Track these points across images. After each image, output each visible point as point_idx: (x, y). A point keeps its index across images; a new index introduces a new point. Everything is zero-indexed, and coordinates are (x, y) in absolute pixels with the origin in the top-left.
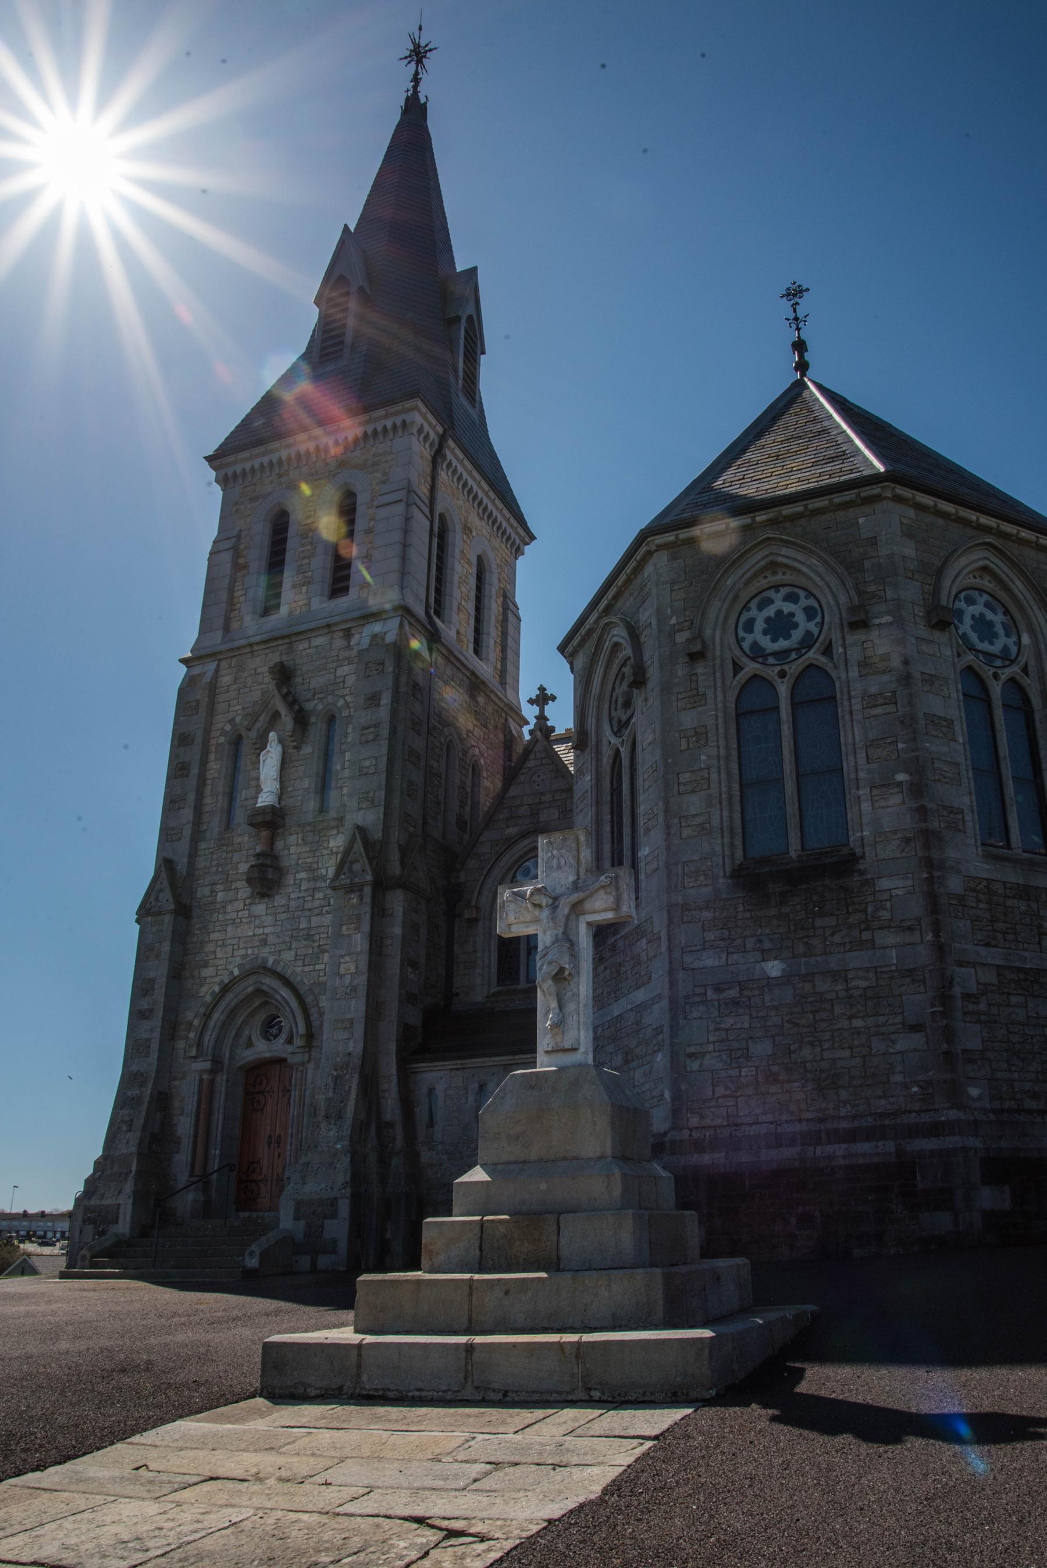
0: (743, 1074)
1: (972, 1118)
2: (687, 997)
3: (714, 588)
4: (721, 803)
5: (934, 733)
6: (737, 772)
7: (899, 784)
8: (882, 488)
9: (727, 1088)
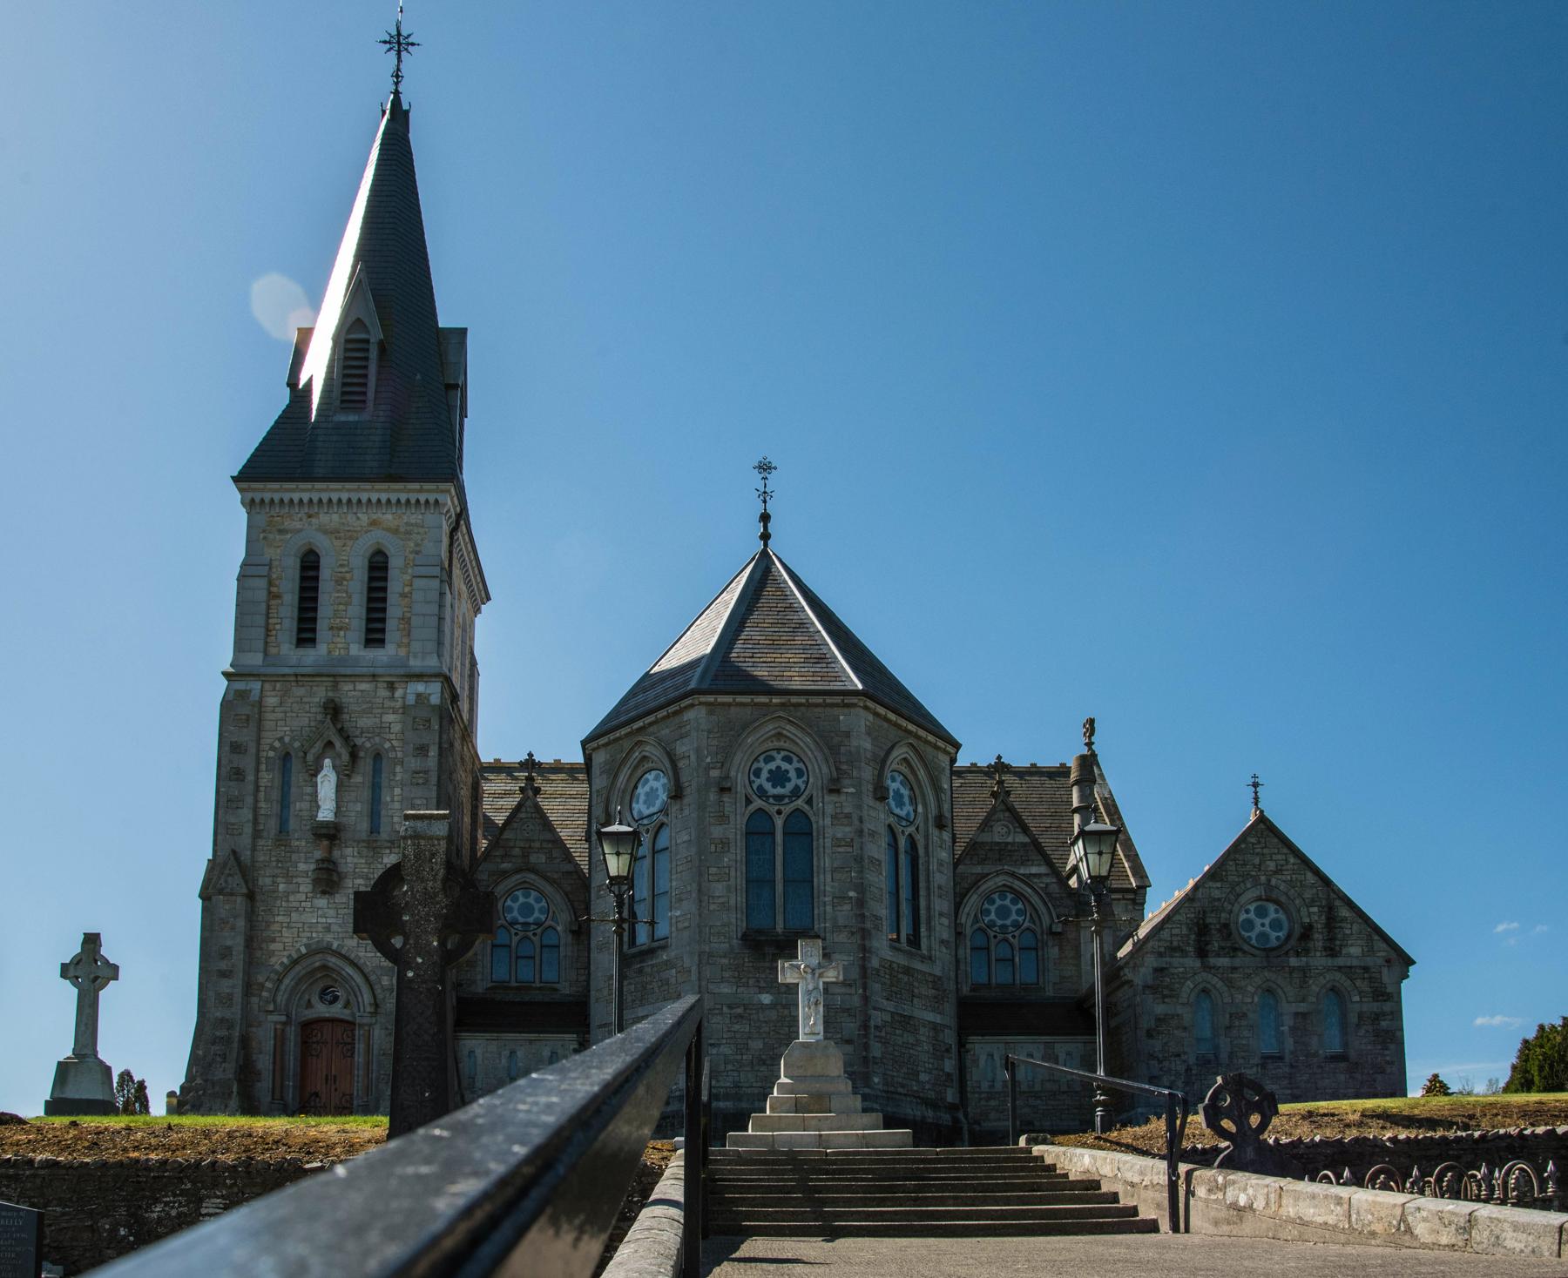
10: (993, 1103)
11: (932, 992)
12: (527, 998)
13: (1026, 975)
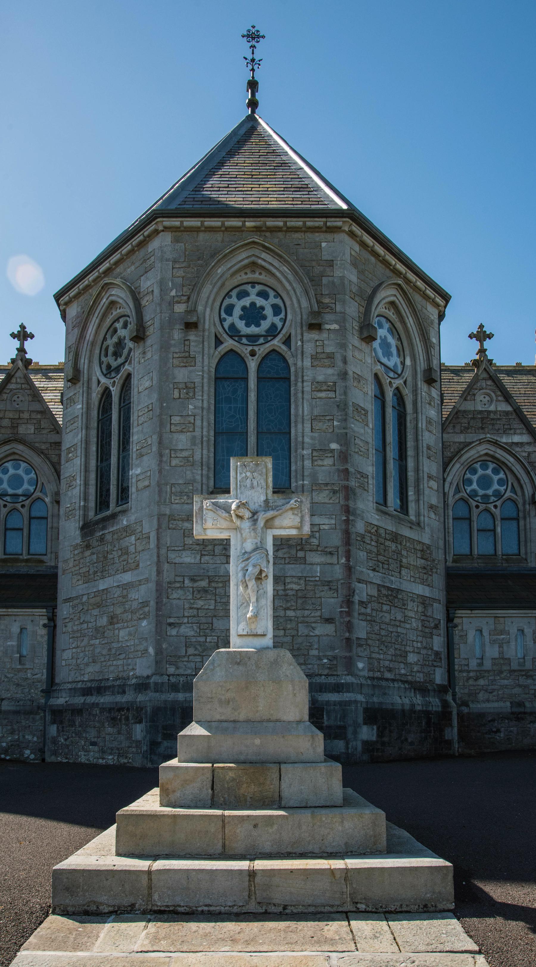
0: (208, 640)
1: (359, 682)
2: (169, 583)
3: (208, 274)
4: (202, 443)
5: (358, 418)
6: (213, 422)
7: (332, 451)
8: (344, 222)
9: (196, 649)
10: (481, 682)
11: (420, 562)
12: (12, 571)
13: (507, 545)
